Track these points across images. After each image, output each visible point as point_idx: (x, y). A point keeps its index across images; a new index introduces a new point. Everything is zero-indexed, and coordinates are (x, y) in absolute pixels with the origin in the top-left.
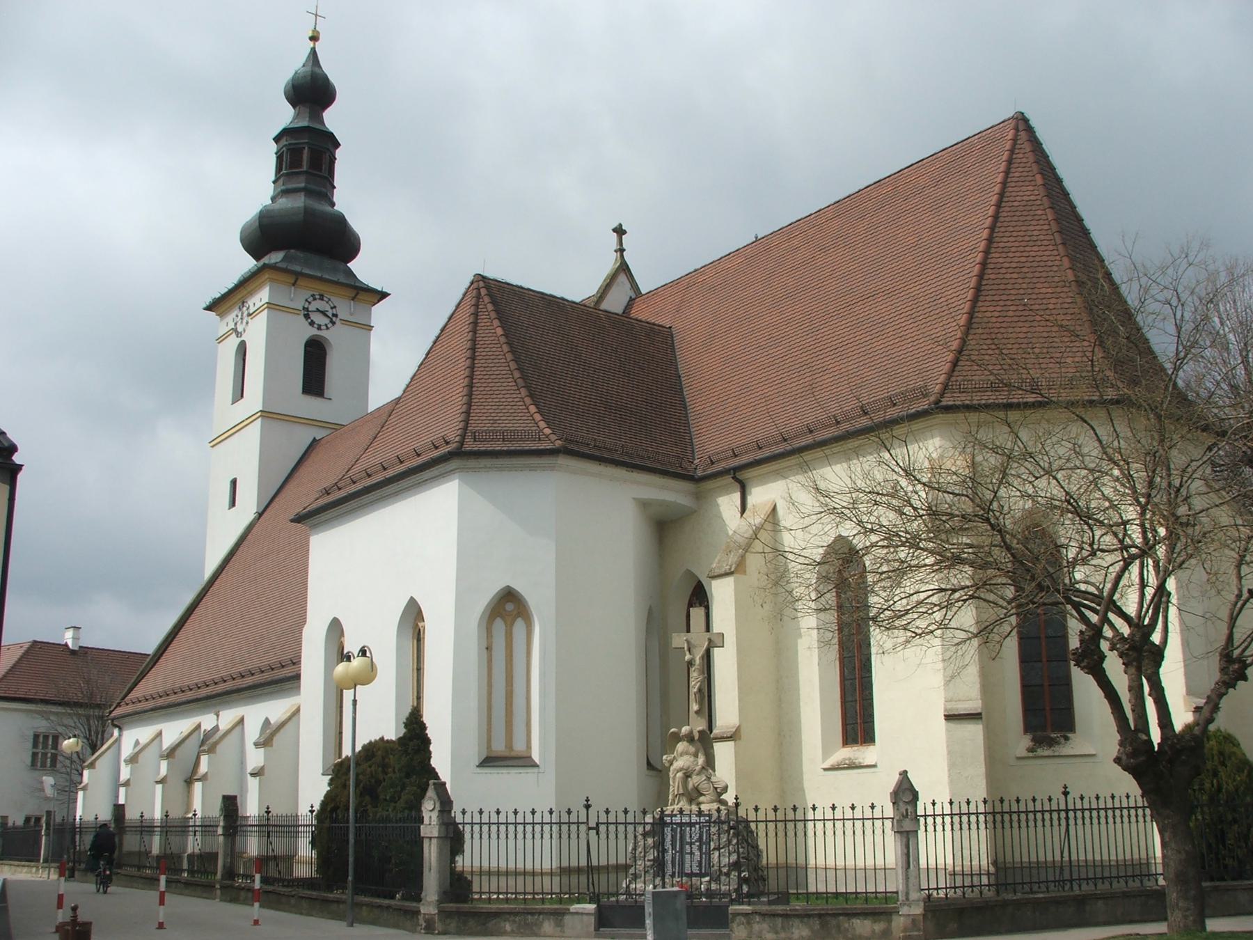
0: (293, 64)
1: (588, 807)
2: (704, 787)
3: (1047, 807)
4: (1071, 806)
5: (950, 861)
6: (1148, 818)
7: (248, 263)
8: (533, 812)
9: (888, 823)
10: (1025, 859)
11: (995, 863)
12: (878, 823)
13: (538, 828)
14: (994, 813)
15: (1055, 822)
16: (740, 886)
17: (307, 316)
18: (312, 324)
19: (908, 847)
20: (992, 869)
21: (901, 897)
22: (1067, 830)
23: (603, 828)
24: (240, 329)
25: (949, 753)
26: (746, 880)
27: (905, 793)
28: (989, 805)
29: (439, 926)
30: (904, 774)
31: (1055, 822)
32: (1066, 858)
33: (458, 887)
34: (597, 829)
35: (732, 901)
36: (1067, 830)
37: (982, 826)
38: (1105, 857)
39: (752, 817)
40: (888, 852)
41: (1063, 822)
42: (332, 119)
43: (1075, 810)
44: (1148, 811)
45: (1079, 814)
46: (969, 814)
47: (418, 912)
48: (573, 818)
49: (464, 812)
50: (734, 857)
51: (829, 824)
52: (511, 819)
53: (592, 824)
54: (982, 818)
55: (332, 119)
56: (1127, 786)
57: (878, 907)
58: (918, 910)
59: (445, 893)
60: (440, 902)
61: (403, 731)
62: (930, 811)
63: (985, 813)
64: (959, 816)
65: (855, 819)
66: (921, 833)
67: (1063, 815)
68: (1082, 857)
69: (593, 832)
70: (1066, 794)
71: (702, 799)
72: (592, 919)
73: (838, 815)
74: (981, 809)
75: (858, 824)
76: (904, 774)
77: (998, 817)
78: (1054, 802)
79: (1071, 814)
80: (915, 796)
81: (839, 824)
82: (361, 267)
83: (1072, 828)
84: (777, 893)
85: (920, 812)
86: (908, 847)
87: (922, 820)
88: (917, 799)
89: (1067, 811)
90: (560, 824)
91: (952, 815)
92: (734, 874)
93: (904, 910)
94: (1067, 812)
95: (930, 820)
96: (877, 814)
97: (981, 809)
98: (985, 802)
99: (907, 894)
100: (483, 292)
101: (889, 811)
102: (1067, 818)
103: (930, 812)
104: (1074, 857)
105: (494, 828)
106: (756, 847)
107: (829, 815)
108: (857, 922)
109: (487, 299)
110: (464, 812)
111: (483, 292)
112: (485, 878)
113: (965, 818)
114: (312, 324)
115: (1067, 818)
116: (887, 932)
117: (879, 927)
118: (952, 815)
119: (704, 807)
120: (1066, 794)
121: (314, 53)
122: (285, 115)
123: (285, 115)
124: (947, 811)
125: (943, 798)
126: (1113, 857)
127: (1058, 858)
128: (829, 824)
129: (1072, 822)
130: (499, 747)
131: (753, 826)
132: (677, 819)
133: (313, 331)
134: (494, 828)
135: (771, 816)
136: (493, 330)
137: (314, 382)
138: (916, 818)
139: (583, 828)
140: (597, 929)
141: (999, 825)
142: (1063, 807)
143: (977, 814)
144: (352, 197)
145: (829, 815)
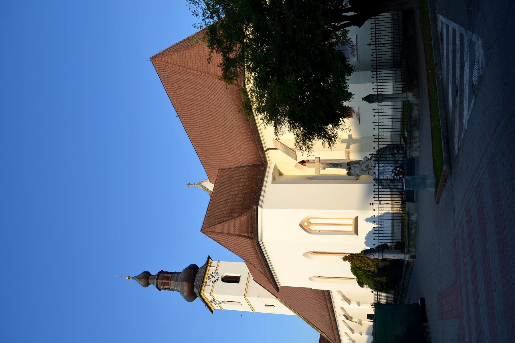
0: (137, 285)
1: (373, 204)
2: (366, 164)
3: (375, 51)
4: (375, 43)
5: (391, 84)
6: (379, 17)
7: (198, 299)
8: (374, 239)
9: (380, 104)
10: (391, 55)
11: (392, 68)
12: (380, 108)
13: (380, 232)
14: (377, 69)
15: (380, 48)
16: (400, 154)
17: (215, 281)
18: (217, 280)
19: (388, 98)
20: (394, 69)
21: (405, 100)
22: (383, 44)
23: (380, 199)
24: (218, 303)
25: (355, 83)
26: (398, 151)
27: (369, 99)
28: (374, 81)
29: (413, 254)
30: (363, 99)
31: (380, 48)
32: (391, 44)
33: (400, 247)
34: (380, 201)
35: (405, 157)
36: (383, 44)
37: (381, 73)
38: (390, 31)
39: (376, 150)
40: (388, 105)
41: (380, 45)
42: (154, 272)
43: (376, 41)
44: (376, 17)
45: (377, 40)
46: (377, 89)
47: (408, 261)
48: (376, 108)
49: (374, 245)
50: (390, 156)
51: (380, 117)
52: (377, 235)
53: (378, 202)
54: (378, 73)
55: (154, 272)
56: (368, 24)
57: (407, 108)
58: (410, 94)
59: (401, 252)
60: (405, 254)
61: (347, 261)
62: (376, 90)
63: (377, 72)
64: (377, 80)
65: (378, 116)
66: (383, 93)
67: (377, 45)
68: (390, 39)
69: (381, 202)
70: (370, 45)
71: (370, 165)
72: (410, 203)
73: (376, 114)
74: (375, 84)
75: (380, 114)
76: (363, 99)
77: (378, 67)
78: (373, 48)
79: (377, 43)
80: (370, 95)
81: (380, 127)
82: (200, 264)
83: (382, 42)
84: (401, 138)
85: (376, 93)
86: (388, 98)
87: (379, 93)
88: (371, 94)
89: (376, 44)
90: (377, 80)
91: (377, 83)
92: (396, 156)
93: (409, 99)
94: (376, 44)
95: (379, 90)
96: (376, 108)
97: (375, 73)
98: (373, 72)
99: (404, 98)
100: (206, 230)
101: (376, 104)
102: (379, 44)
103: (376, 90)
104: (390, 42)
105: (379, 235)
106: (386, 148)
107: (377, 130)
108: (413, 115)
109: (208, 229)
110: (374, 245)
111: (206, 230)
112: (395, 232)
113: (378, 78)
114: (217, 280)
115: (379, 44)
116: (417, 105)
117: (415, 108)
118: (377, 83)
119: (373, 165)
120: (370, 45)
121: (133, 278)
122: (152, 287)
123: (152, 287)
124: (375, 84)
125: (371, 86)
126: (390, 29)
127: (390, 47)
128: (380, 111)
129: (380, 42)
130: (351, 229)
131: (379, 214)
132: (377, 174)
133: (220, 279)
134: (379, 235)
135: (377, 193)
136: (217, 228)
137: (235, 280)
138: (378, 95)
139: (380, 206)
140: (414, 202)
141: (381, 67)
142: (375, 46)
143: (377, 74)
144: (180, 267)
145: (376, 124)
